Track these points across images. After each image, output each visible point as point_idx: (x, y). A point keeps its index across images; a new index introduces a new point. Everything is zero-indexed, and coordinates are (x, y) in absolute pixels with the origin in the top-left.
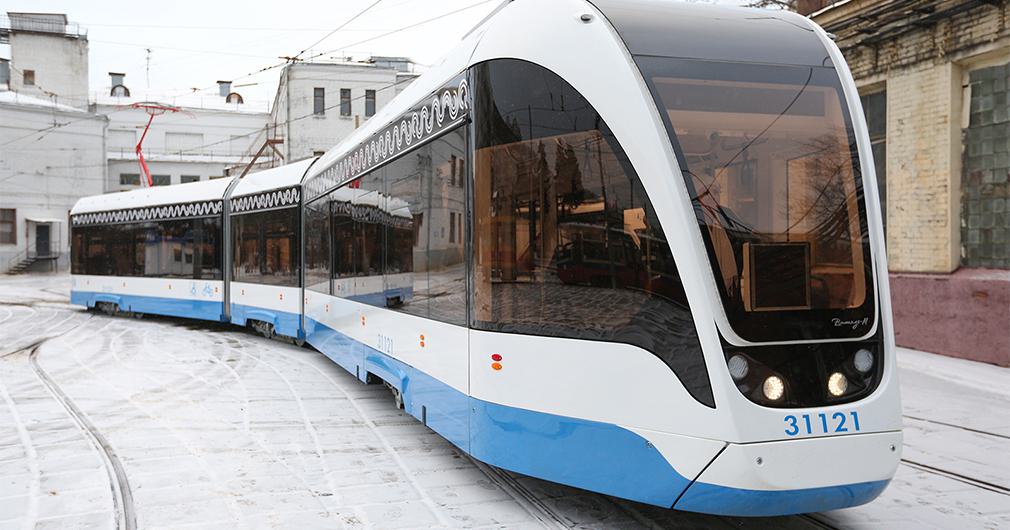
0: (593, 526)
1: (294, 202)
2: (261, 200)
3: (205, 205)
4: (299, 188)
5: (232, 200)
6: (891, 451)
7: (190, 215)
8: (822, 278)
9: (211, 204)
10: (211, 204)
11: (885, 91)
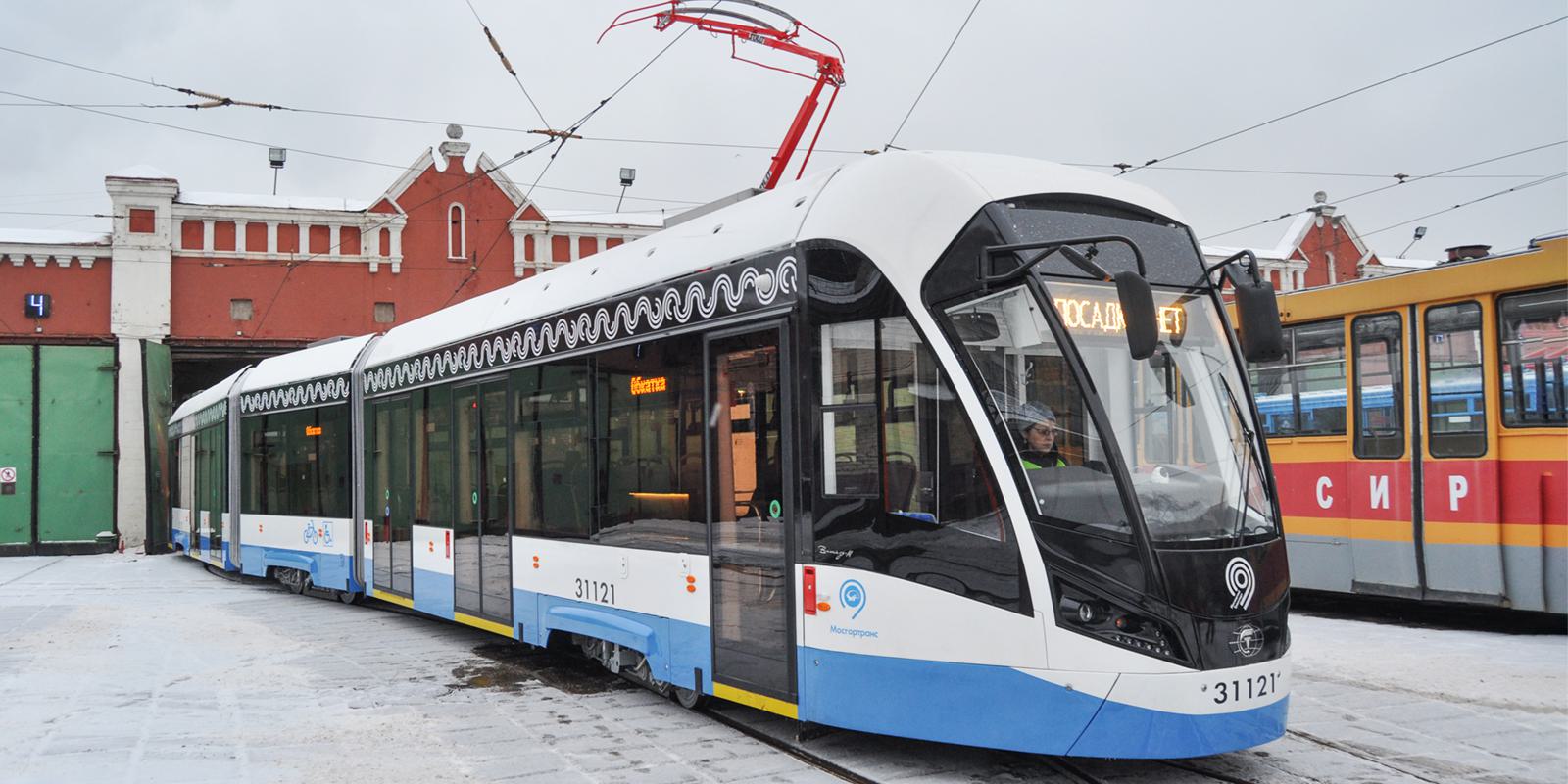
0: (929, 780)
1: (341, 397)
2: (254, 401)
3: (623, 308)
4: (347, 377)
5: (366, 372)
6: (1201, 691)
7: (666, 324)
8: (841, 481)
9: (643, 305)
10: (643, 305)
11: (883, 275)
